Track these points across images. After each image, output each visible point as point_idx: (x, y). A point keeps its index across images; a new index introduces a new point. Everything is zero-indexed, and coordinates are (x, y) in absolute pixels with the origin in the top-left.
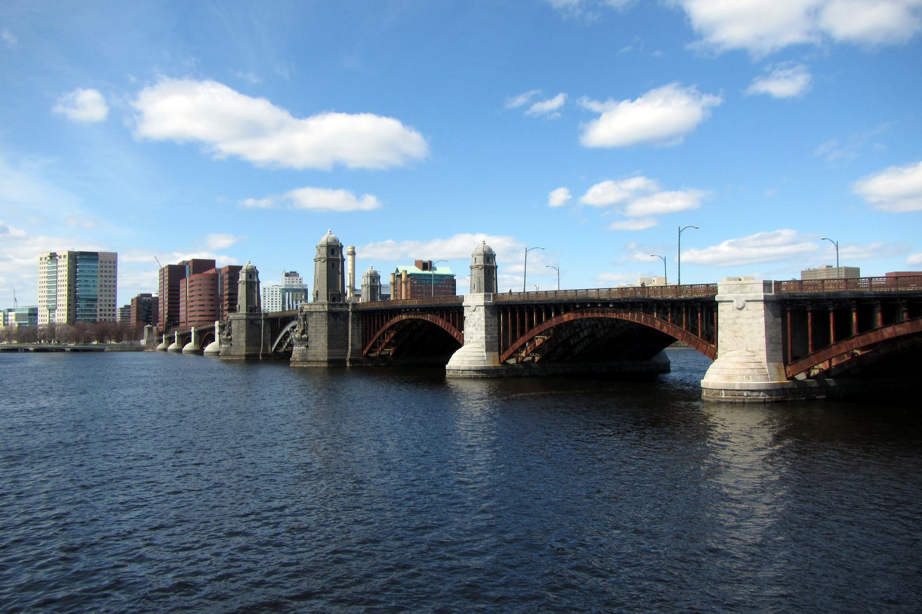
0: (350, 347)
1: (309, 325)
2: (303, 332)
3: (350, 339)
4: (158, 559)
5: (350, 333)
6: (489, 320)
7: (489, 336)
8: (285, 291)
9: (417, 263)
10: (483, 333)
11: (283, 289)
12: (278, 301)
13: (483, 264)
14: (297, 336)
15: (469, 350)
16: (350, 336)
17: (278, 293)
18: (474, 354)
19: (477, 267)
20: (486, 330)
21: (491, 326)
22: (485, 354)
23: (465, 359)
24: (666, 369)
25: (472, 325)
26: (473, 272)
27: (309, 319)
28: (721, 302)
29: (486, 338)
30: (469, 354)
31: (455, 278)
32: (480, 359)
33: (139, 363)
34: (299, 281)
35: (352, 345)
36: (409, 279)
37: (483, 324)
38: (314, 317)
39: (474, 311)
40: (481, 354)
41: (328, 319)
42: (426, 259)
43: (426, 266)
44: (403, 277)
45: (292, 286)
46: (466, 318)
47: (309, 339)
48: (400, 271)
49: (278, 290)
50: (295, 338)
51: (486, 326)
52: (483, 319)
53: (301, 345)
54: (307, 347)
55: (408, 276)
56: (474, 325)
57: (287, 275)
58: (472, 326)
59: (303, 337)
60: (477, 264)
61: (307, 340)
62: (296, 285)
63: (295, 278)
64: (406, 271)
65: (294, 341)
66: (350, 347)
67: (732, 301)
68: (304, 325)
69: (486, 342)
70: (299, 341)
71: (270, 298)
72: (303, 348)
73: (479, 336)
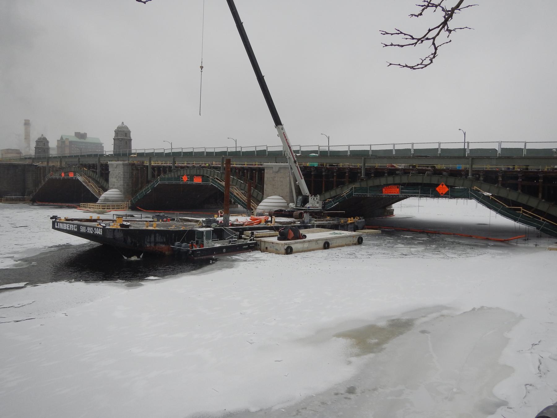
7: (126, 185)
37: (122, 176)
39: (116, 168)
42: (82, 132)
58: (114, 177)
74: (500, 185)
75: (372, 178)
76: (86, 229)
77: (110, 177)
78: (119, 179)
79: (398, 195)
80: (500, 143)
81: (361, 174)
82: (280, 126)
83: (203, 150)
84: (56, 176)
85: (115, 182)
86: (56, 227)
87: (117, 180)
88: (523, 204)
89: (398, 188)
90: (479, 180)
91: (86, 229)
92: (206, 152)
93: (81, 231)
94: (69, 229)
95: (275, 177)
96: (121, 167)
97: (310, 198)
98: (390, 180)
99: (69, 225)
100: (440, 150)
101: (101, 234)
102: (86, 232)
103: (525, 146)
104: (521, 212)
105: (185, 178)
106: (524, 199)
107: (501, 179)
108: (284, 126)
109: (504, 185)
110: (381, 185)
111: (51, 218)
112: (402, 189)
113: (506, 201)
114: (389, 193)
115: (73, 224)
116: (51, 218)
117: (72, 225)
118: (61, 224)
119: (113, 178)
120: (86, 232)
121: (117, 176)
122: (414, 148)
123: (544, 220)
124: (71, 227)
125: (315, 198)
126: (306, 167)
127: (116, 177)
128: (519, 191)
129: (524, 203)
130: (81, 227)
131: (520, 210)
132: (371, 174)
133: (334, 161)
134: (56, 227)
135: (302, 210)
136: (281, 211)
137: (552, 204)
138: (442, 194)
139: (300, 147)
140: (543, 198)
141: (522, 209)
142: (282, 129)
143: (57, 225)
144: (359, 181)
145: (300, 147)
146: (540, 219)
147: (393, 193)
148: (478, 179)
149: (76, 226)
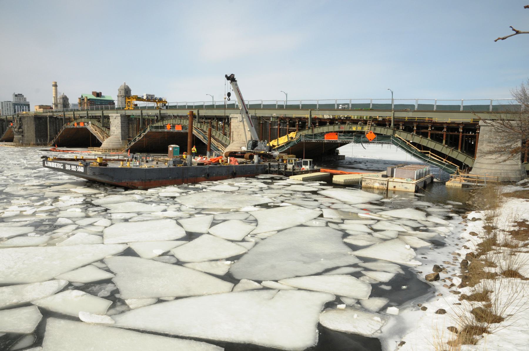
0: (49, 137)
1: (23, 124)
2: (20, 128)
3: (49, 132)
4: (40, 298)
5: (48, 129)
6: (123, 124)
7: (123, 132)
8: (15, 105)
9: (94, 93)
10: (120, 131)
11: (14, 104)
12: (11, 110)
13: (124, 95)
14: (16, 130)
15: (112, 139)
16: (48, 131)
17: (11, 106)
18: (115, 141)
19: (121, 96)
20: (122, 129)
21: (124, 127)
22: (121, 141)
23: (111, 144)
24: (338, 153)
25: (114, 126)
26: (119, 99)
27: (23, 121)
28: (232, 118)
29: (122, 133)
30: (112, 141)
31: (114, 102)
32: (118, 144)
33: (476, 184)
34: (24, 99)
35: (50, 136)
36: (89, 101)
37: (120, 126)
38: (26, 119)
39: (115, 119)
40: (119, 141)
41: (35, 120)
42: (98, 91)
43: (98, 95)
44: (85, 100)
45: (20, 102)
46: (111, 122)
47: (24, 132)
48: (84, 97)
49: (11, 104)
50: (15, 131)
51: (122, 127)
52: (120, 123)
53: (19, 135)
54: (23, 136)
55: (88, 100)
56: (115, 127)
57: (16, 96)
58: (114, 126)
59: (20, 130)
60: (121, 95)
61: (22, 132)
62: (22, 102)
63: (21, 98)
64: (87, 97)
65: (14, 132)
66: (49, 137)
67: (237, 118)
68: (20, 124)
69: (122, 135)
70: (17, 132)
71: (6, 108)
72: (20, 136)
73: (118, 132)
74: (415, 133)
75: (317, 126)
76: (71, 167)
77: (111, 126)
78: (118, 128)
79: (336, 141)
80: (301, 101)
81: (308, 123)
82: (234, 83)
83: (487, 103)
84: (70, 126)
85: (115, 130)
86: (46, 165)
87: (117, 129)
88: (431, 149)
89: (336, 135)
90: (399, 129)
91: (71, 167)
92: (373, 104)
93: (66, 169)
94: (56, 167)
95: (239, 126)
96: (119, 118)
97: (259, 143)
98: (331, 128)
99: (56, 163)
100: (371, 105)
101: (83, 171)
102: (71, 169)
103: (249, 102)
104: (429, 155)
105: (168, 127)
106: (432, 144)
107: (462, 131)
108: (238, 83)
109: (418, 133)
110: (323, 133)
111: (42, 158)
112: (340, 136)
113: (419, 146)
114: (329, 139)
115: (60, 163)
116: (42, 158)
117: (59, 164)
118: (50, 162)
119: (113, 127)
120: (71, 169)
121: (116, 125)
122: (493, 105)
123: (446, 162)
124: (58, 165)
125: (264, 143)
126: (259, 119)
127: (115, 127)
128: (429, 138)
129: (432, 148)
130: (66, 165)
131: (428, 153)
132: (316, 123)
133: (427, 116)
134: (46, 165)
135: (252, 152)
136: (235, 152)
137: (453, 148)
138: (371, 140)
139: (262, 101)
140: (446, 144)
141: (430, 153)
142: (236, 85)
143: (47, 164)
144: (307, 129)
145: (262, 101)
146: (443, 160)
147: (332, 139)
148: (398, 128)
149: (62, 164)
